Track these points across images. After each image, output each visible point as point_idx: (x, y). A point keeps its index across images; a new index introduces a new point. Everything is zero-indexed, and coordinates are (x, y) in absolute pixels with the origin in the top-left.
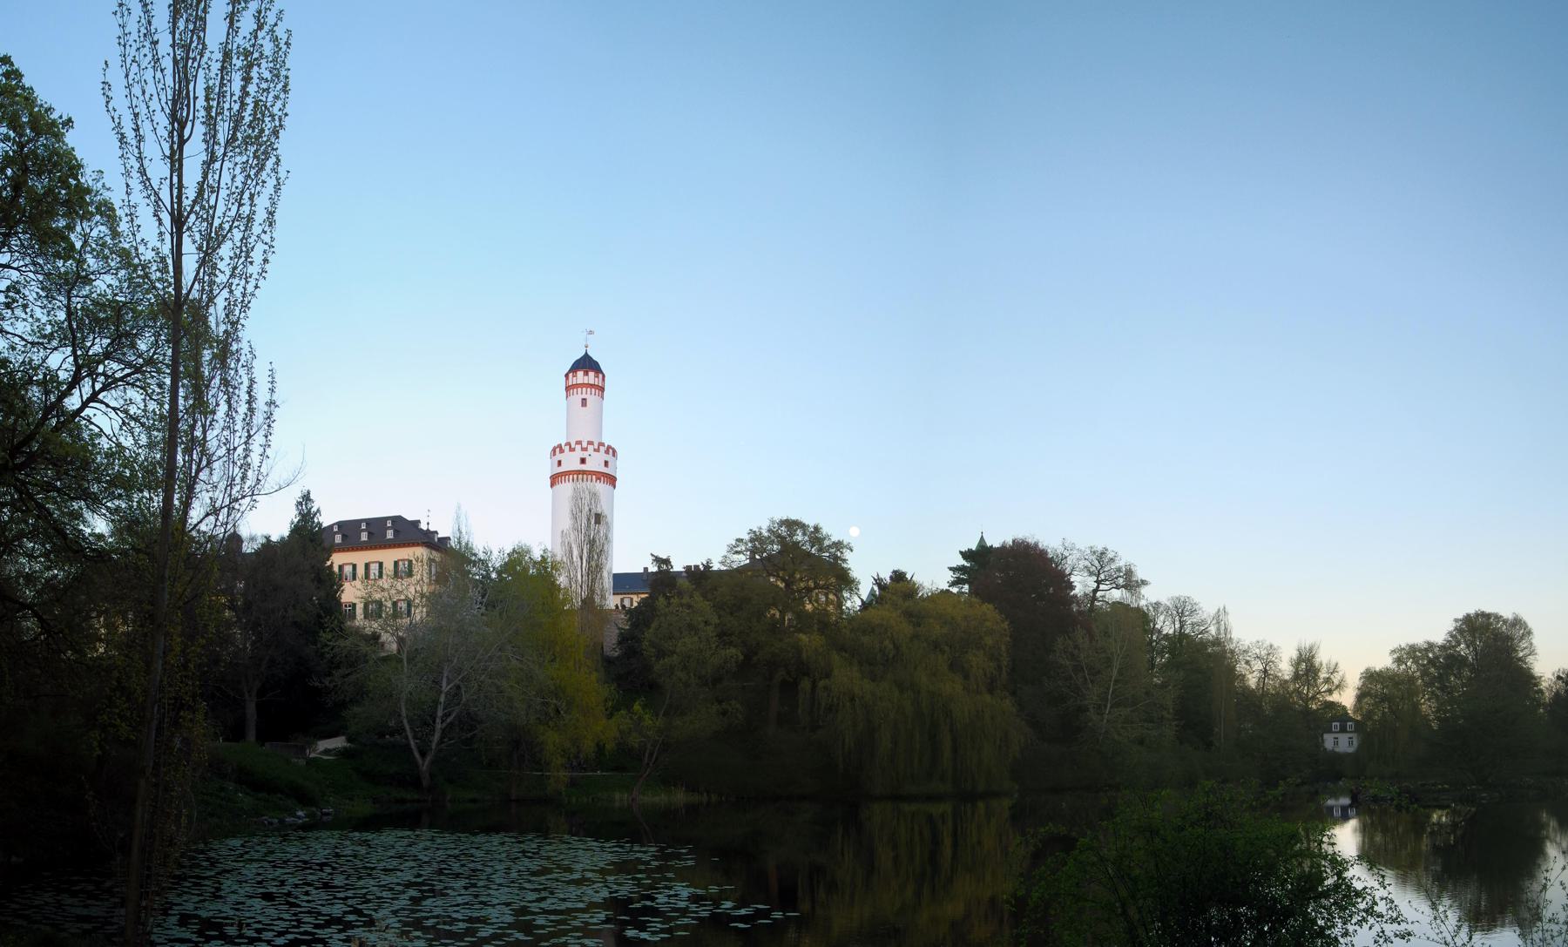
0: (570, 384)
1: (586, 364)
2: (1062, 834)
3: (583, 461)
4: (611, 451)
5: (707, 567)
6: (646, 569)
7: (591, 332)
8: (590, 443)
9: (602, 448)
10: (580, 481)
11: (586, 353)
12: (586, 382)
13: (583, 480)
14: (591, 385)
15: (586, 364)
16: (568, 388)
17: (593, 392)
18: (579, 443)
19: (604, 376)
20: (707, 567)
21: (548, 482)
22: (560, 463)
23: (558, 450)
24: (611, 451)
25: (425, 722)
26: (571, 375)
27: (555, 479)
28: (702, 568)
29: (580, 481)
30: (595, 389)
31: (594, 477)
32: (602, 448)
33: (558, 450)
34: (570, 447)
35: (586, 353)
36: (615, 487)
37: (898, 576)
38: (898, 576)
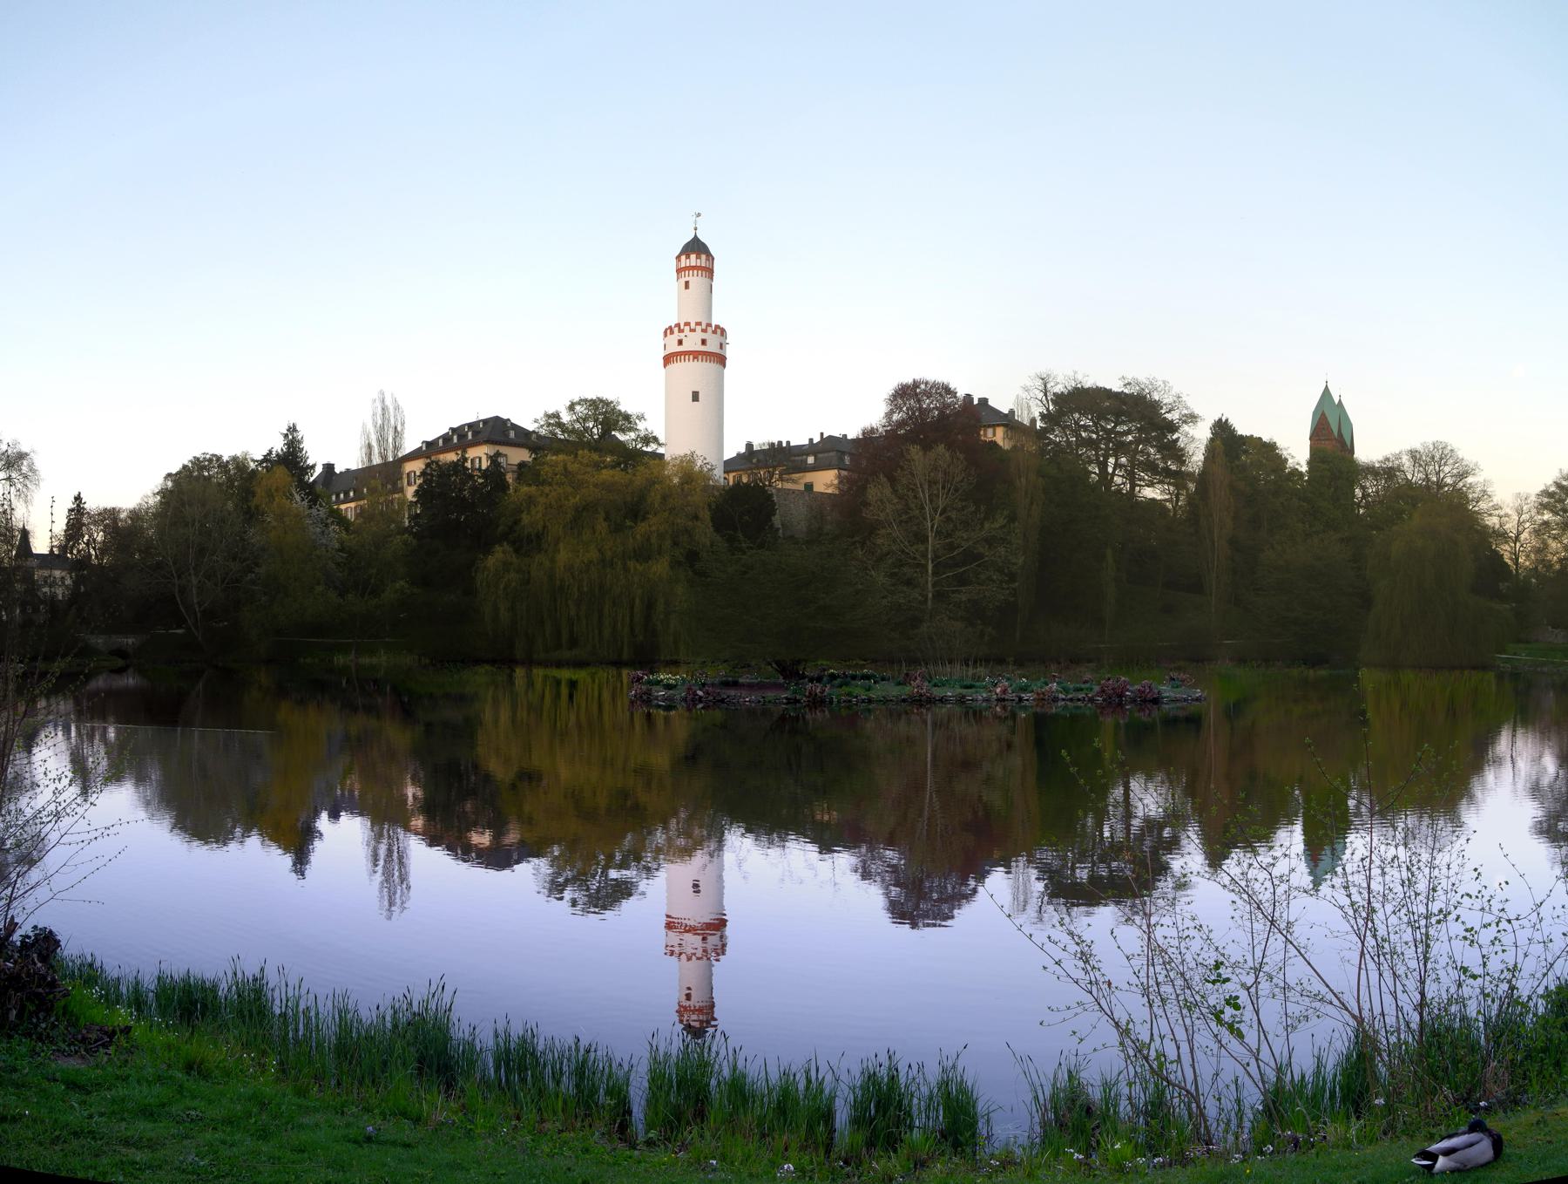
0: (683, 265)
1: (695, 247)
2: (1171, 715)
3: (704, 342)
4: (719, 331)
5: (291, 459)
6: (811, 440)
7: (699, 215)
8: (698, 324)
9: (709, 328)
10: (687, 360)
11: (696, 236)
12: (698, 264)
13: (689, 360)
14: (693, 267)
15: (695, 247)
16: (679, 271)
17: (700, 275)
18: (687, 324)
19: (713, 259)
20: (291, 459)
21: (662, 361)
22: (680, 342)
23: (668, 331)
24: (719, 331)
25: (147, 513)
26: (683, 257)
27: (668, 360)
28: (784, 445)
29: (687, 360)
30: (706, 271)
31: (691, 357)
32: (709, 328)
33: (668, 331)
34: (679, 328)
35: (696, 236)
36: (724, 366)
37: (333, 465)
38: (333, 465)
